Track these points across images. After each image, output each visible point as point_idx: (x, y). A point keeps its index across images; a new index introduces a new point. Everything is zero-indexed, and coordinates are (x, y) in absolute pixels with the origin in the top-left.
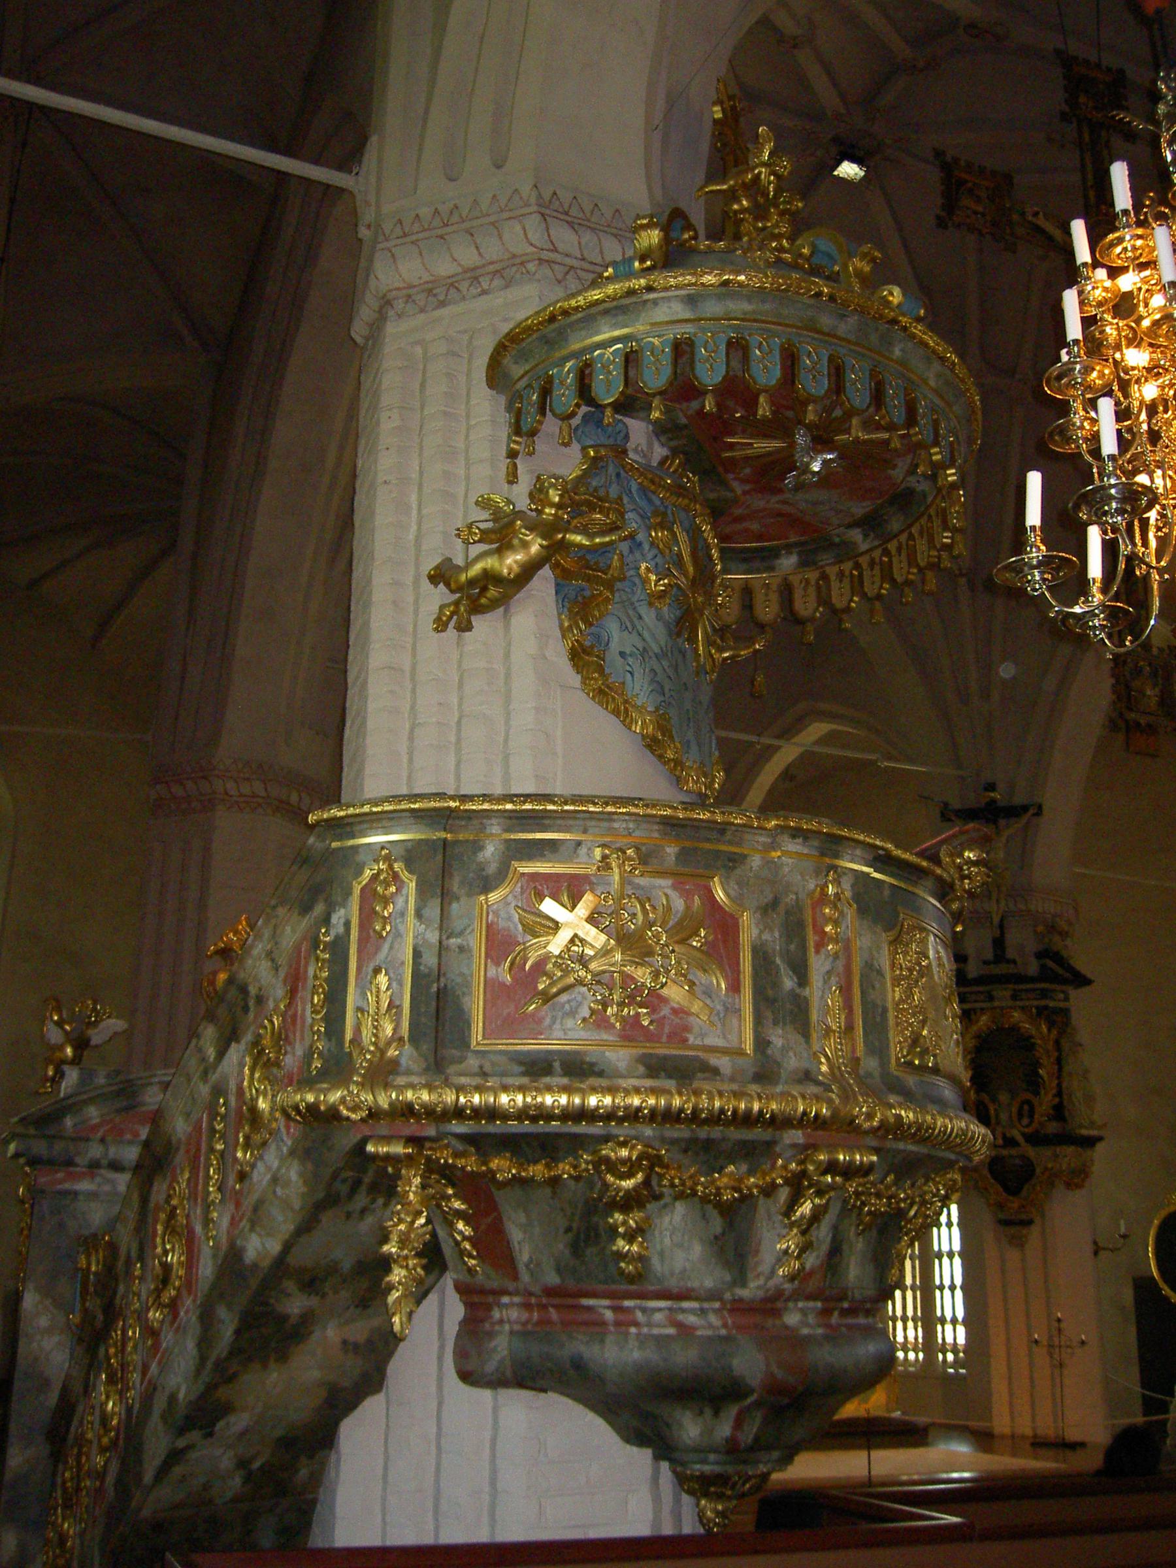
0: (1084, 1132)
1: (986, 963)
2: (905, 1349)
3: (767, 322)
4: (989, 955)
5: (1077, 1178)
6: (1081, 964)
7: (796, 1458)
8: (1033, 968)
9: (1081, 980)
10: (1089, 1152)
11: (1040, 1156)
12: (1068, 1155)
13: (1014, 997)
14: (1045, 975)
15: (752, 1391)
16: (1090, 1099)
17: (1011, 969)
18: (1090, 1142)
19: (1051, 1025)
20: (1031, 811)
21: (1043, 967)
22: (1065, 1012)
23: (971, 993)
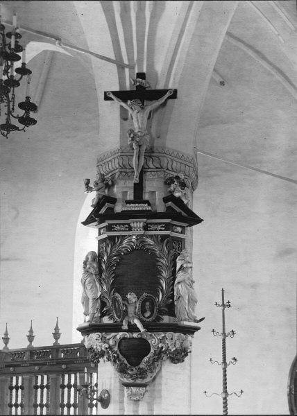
0: (186, 323)
1: (129, 202)
2: (69, 406)
3: (259, 10)
4: (130, 197)
5: (179, 356)
6: (197, 209)
7: (52, 345)
8: (161, 208)
9: (194, 220)
10: (189, 338)
11: (154, 341)
12: (172, 341)
13: (146, 228)
14: (169, 213)
15: (121, 107)
16: (193, 301)
17: (145, 207)
18: (191, 331)
19: (170, 248)
20: (168, 94)
21: (169, 208)
22: (180, 242)
23: (116, 225)
